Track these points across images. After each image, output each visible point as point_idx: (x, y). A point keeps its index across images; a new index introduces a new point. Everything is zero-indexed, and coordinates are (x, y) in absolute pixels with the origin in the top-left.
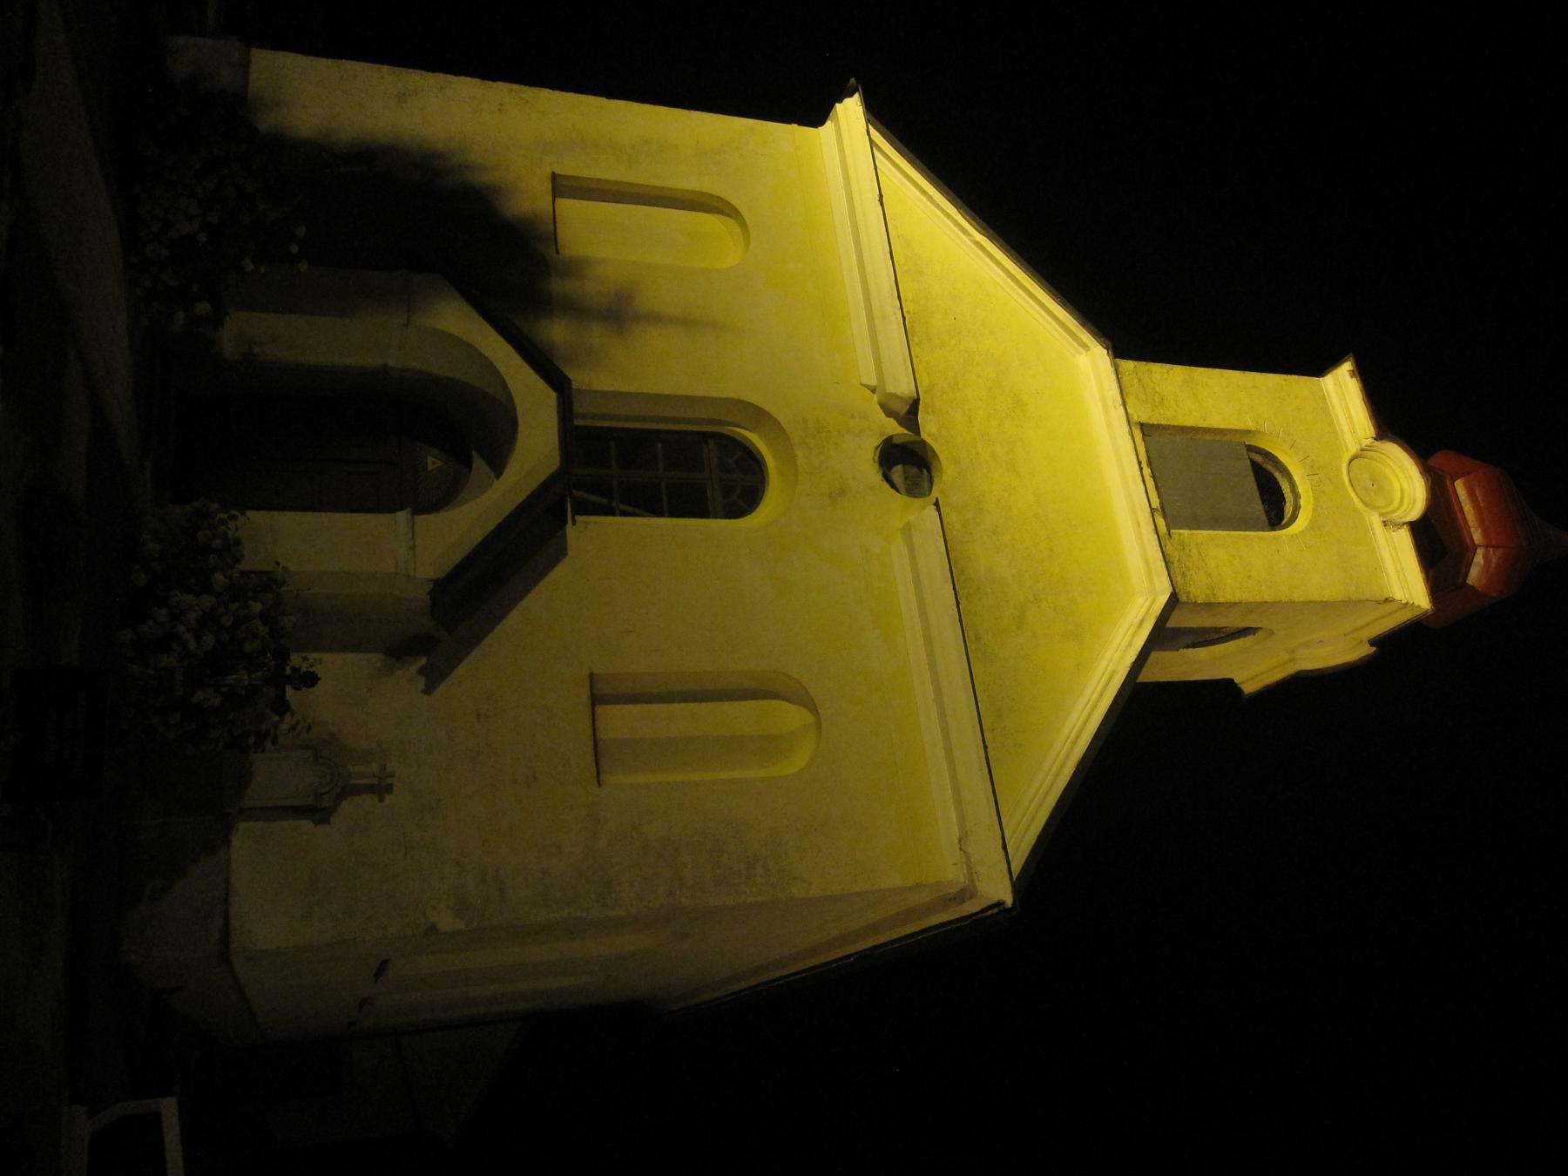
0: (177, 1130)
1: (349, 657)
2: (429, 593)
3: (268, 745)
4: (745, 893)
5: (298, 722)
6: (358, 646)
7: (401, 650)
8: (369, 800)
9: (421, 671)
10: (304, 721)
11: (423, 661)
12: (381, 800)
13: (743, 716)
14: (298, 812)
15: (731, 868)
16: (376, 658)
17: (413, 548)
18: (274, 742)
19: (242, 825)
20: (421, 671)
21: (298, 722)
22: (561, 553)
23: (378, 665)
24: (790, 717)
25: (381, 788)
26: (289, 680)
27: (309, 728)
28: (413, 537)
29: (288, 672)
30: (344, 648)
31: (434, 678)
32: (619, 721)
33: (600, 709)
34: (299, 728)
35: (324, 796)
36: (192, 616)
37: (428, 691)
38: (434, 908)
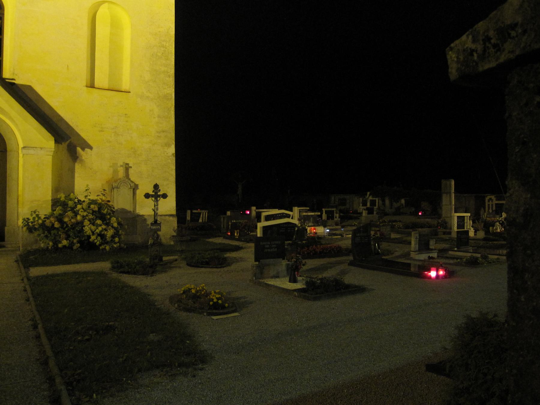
0: (462, 214)
1: (76, 175)
2: (61, 144)
3: (110, 204)
4: (171, 51)
5: (102, 194)
6: (72, 171)
7: (74, 156)
8: (131, 171)
9: (83, 149)
10: (102, 191)
11: (79, 149)
12: (131, 167)
13: (102, 32)
14: (134, 194)
15: (163, 53)
16: (77, 166)
17: (41, 148)
18: (109, 201)
19: (137, 211)
20: (83, 149)
21: (102, 194)
22: (30, 88)
23: (80, 165)
24: (103, 12)
25: (127, 168)
26: (156, 193)
27: (104, 190)
28: (36, 148)
29: (154, 193)
30: (73, 177)
31: (86, 145)
32: (101, 79)
33: (96, 85)
34: (104, 193)
35: (131, 186)
36: (93, 228)
37: (91, 148)
38: (167, 154)
